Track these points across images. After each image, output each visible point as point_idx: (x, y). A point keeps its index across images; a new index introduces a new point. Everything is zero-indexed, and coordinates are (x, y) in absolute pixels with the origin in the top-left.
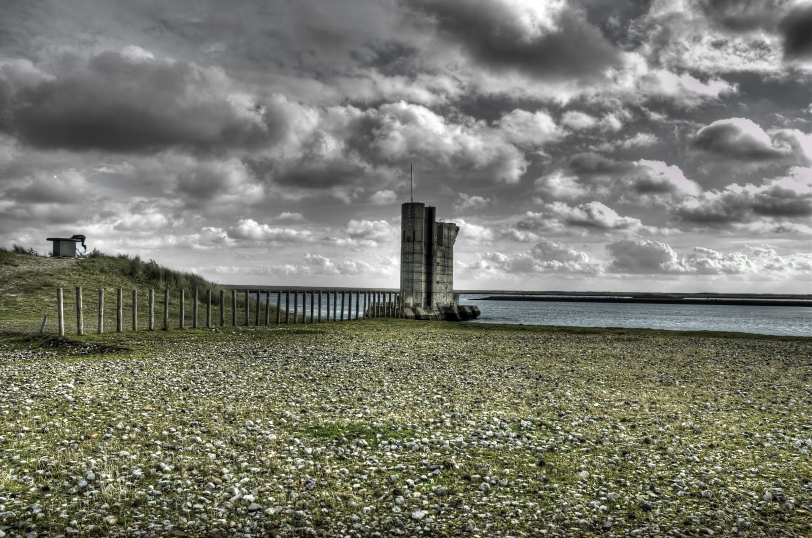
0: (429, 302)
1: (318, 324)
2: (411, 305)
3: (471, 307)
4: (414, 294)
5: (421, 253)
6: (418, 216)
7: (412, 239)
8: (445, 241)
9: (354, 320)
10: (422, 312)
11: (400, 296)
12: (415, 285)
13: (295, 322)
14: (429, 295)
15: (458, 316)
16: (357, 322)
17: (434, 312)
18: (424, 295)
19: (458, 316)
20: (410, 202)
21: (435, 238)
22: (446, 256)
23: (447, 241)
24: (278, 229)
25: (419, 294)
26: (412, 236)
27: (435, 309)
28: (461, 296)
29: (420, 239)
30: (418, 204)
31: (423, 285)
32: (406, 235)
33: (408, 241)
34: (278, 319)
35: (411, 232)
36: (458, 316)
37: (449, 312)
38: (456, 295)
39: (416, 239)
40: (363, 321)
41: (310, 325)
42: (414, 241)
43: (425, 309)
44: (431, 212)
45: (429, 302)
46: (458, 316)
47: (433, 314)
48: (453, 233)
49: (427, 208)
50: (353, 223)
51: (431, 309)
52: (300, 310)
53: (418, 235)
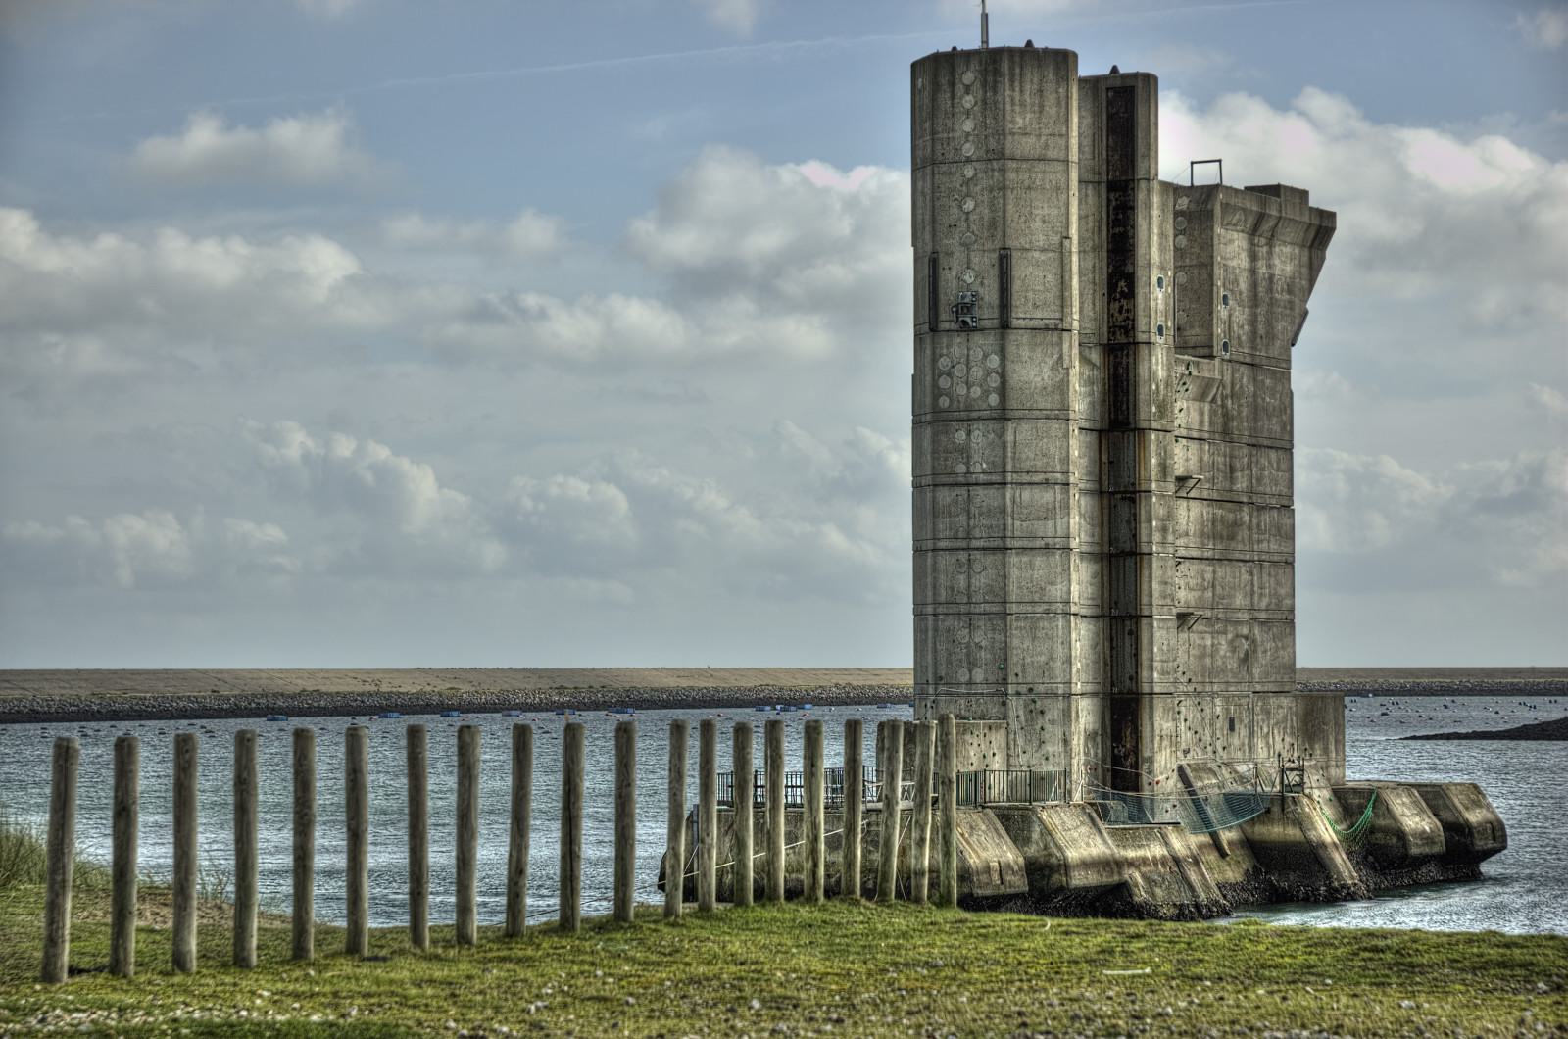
0: (1121, 771)
1: (346, 966)
2: (998, 787)
3: (1433, 797)
4: (1016, 707)
5: (1062, 415)
6: (1028, 145)
7: (988, 314)
8: (1230, 316)
9: (600, 927)
10: (1080, 843)
11: (911, 727)
12: (1020, 643)
13: (179, 962)
14: (1123, 711)
15: (1340, 859)
16: (622, 942)
17: (1159, 832)
18: (1085, 715)
19: (1342, 864)
20: (971, 41)
21: (1157, 298)
22: (1242, 427)
23: (1241, 316)
24: (1084, 461)
25: (1054, 711)
26: (990, 294)
27: (1166, 813)
28: (1355, 708)
29: (1048, 314)
30: (1028, 55)
31: (1081, 640)
32: (949, 279)
33: (965, 328)
34: (52, 941)
35: (984, 261)
36: (1342, 864)
37: (1277, 831)
38: (1320, 709)
39: (1020, 314)
40: (668, 936)
41: (293, 980)
42: (1005, 326)
43: (1098, 813)
44: (1123, 108)
45: (1121, 771)
46: (1340, 859)
47: (1157, 850)
48: (1284, 261)
49: (1092, 84)
50: (724, 179)
51: (1139, 812)
52: (213, 845)
53: (1032, 278)
